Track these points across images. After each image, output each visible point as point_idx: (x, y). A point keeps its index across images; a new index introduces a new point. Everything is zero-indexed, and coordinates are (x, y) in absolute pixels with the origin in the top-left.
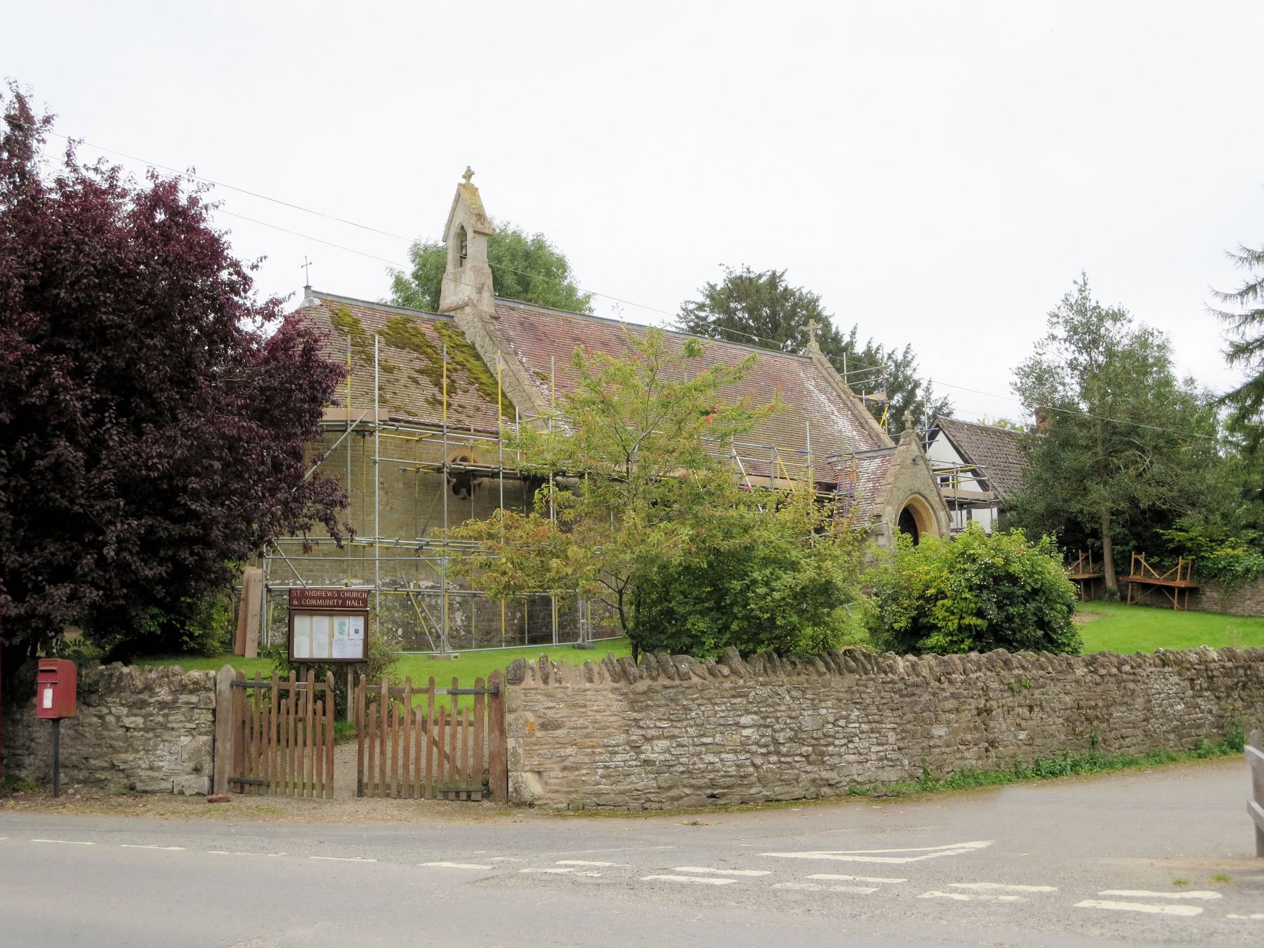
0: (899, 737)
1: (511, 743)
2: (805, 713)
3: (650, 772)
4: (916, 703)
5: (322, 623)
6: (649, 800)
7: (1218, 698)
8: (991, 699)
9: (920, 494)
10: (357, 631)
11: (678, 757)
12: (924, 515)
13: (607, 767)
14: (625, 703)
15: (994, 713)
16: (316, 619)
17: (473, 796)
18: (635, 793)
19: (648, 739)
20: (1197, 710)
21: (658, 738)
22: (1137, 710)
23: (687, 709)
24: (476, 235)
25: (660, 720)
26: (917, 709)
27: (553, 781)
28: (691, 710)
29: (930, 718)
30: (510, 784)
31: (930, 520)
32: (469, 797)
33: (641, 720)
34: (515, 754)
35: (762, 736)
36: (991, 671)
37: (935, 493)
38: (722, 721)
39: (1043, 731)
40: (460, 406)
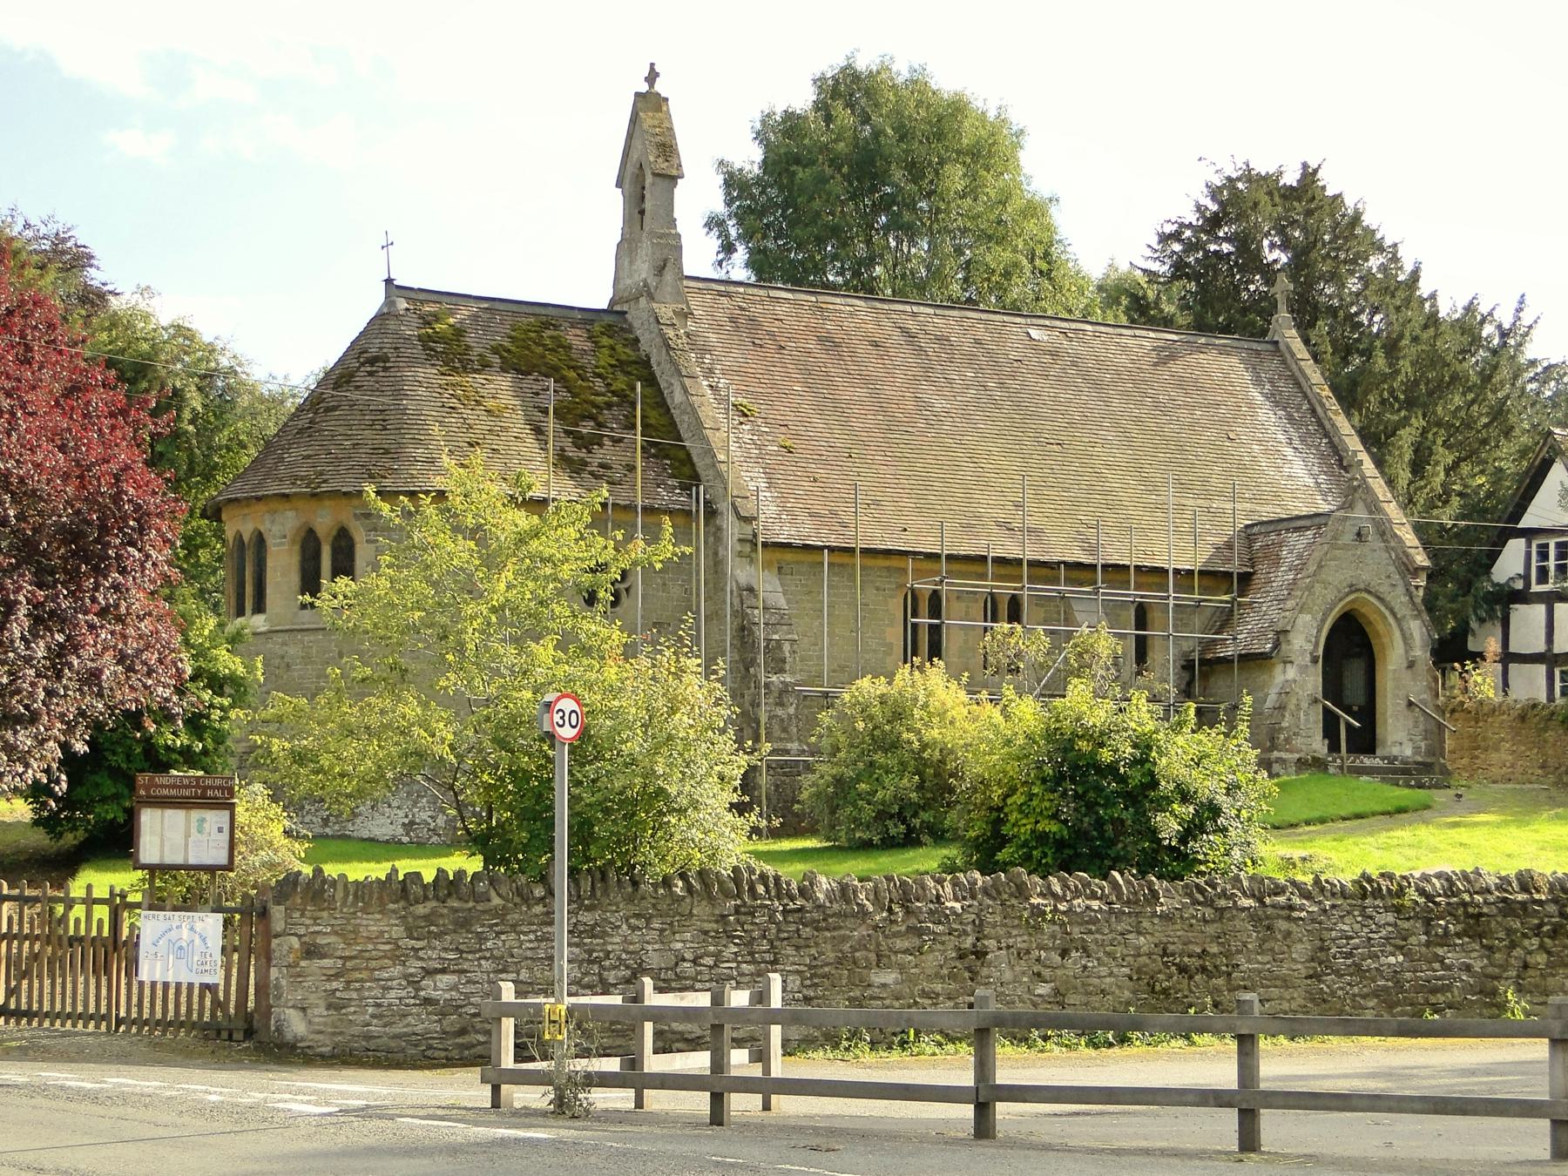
0: (808, 982)
1: (274, 973)
2: (650, 947)
3: (430, 1013)
4: (844, 939)
5: (176, 817)
6: (430, 1047)
7: (1490, 948)
8: (986, 937)
9: (1369, 592)
10: (220, 830)
11: (467, 995)
12: (1380, 628)
13: (378, 1005)
14: (402, 929)
15: (989, 957)
16: (169, 812)
17: (235, 1036)
18: (414, 1038)
19: (429, 973)
20: (1437, 965)
21: (443, 971)
22: (1294, 960)
23: (481, 938)
24: (658, 180)
25: (445, 950)
26: (846, 947)
27: (317, 1020)
28: (487, 939)
29: (867, 959)
30: (273, 1022)
31: (1390, 633)
32: (230, 1036)
33: (421, 949)
34: (278, 987)
35: (586, 974)
36: (994, 899)
37: (1400, 590)
38: (529, 954)
39: (1083, 984)
40: (602, 466)
